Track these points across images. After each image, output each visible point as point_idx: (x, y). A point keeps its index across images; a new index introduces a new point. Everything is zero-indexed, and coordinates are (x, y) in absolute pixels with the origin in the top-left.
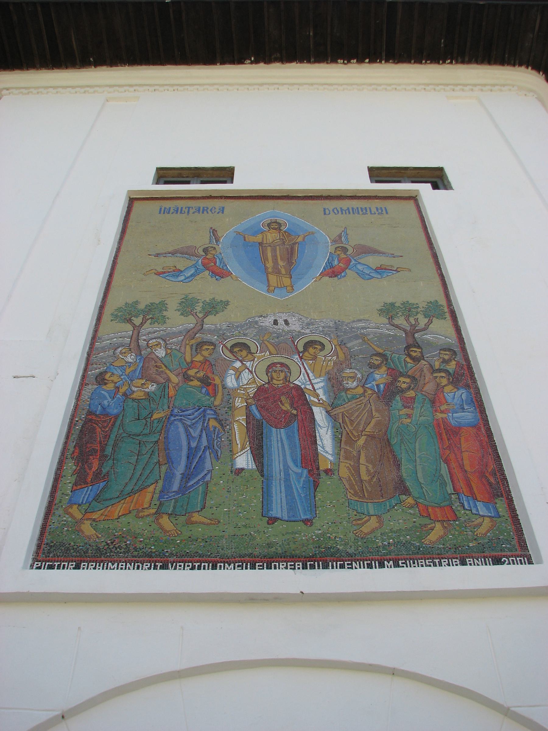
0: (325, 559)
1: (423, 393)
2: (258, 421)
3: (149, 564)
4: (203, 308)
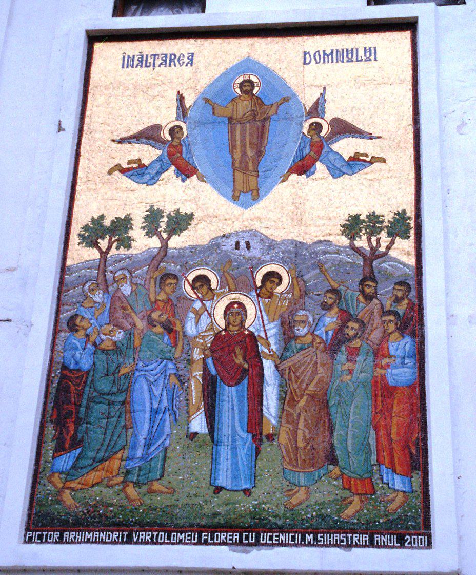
0: (257, 530)
1: (369, 342)
2: (213, 376)
3: (118, 533)
4: (168, 224)
